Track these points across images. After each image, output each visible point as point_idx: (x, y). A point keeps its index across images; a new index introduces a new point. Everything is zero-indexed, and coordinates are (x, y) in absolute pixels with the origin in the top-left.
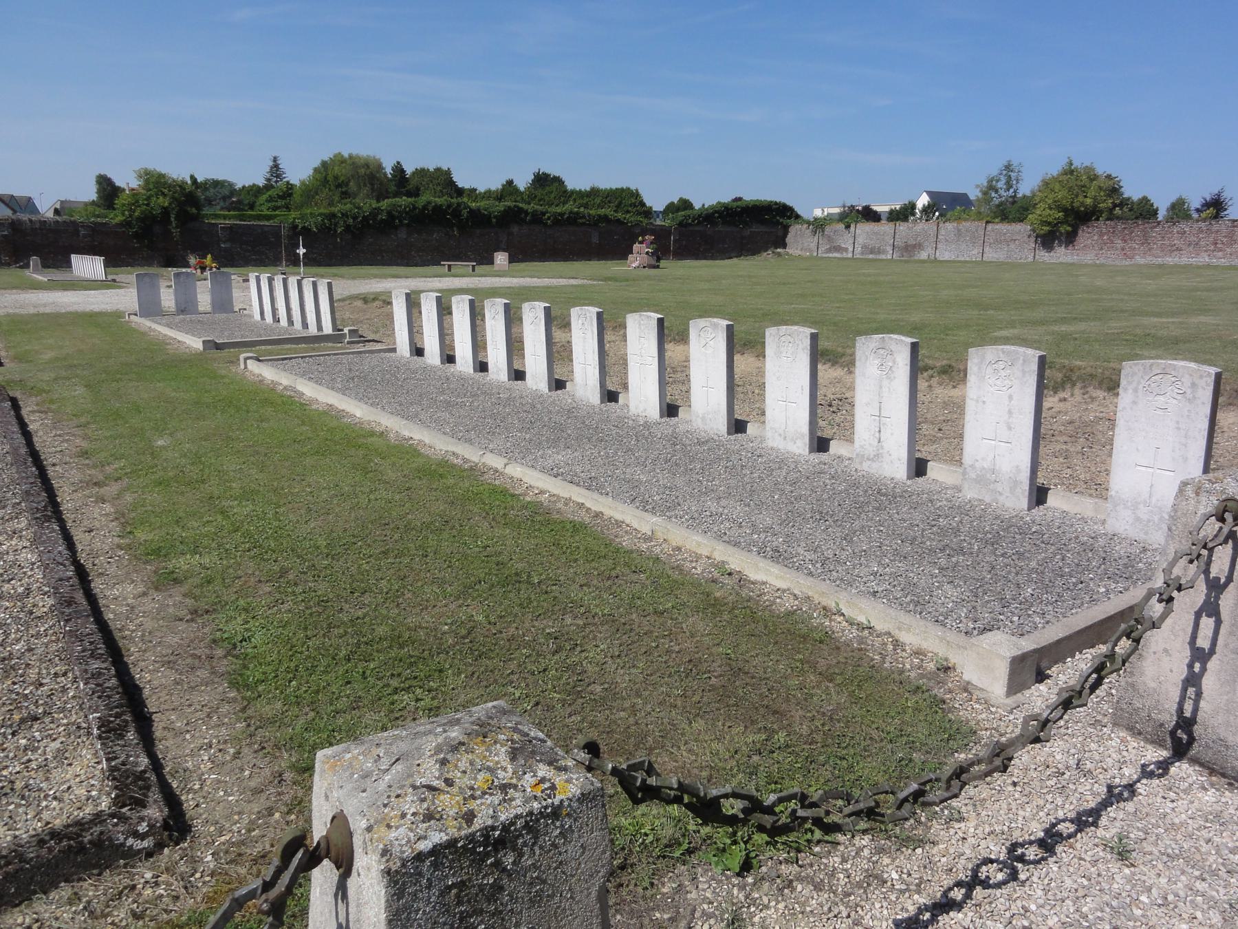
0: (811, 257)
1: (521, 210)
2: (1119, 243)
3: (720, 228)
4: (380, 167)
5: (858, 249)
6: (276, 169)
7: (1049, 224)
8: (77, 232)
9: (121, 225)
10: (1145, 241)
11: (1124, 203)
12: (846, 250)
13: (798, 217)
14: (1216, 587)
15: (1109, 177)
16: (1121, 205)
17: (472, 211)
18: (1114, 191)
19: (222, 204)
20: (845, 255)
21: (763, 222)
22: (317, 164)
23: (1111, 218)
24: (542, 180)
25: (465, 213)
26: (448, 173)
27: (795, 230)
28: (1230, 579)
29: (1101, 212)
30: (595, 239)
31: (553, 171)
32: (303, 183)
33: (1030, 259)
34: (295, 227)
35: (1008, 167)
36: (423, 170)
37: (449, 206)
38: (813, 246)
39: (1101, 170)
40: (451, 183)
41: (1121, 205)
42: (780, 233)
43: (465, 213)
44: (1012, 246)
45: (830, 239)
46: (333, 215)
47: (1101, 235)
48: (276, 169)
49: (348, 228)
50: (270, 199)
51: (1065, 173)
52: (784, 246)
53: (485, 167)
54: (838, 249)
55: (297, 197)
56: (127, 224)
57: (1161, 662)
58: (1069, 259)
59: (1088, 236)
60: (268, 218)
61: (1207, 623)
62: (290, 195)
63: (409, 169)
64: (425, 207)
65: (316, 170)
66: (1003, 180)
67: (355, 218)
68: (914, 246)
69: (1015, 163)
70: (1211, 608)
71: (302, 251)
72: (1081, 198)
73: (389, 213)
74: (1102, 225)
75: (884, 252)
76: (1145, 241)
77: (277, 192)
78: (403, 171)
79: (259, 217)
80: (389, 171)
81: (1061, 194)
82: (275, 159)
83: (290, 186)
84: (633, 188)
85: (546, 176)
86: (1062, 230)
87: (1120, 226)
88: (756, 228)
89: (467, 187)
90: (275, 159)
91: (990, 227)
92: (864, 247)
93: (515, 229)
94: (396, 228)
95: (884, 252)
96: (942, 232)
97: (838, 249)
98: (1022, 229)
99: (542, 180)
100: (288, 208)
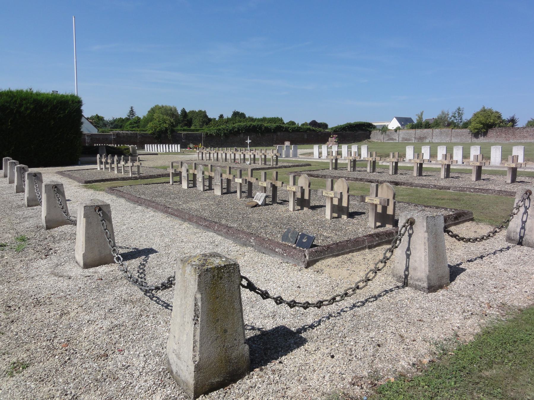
0: (381, 143)
1: (281, 127)
2: (504, 135)
3: (348, 132)
4: (176, 110)
5: (400, 139)
6: (132, 112)
7: (477, 129)
8: (137, 136)
9: (151, 134)
10: (514, 134)
11: (503, 121)
12: (396, 140)
13: (374, 127)
14: (526, 208)
15: (497, 112)
16: (502, 122)
17: (265, 127)
18: (499, 117)
19: (111, 126)
20: (395, 141)
21: (362, 130)
22: (149, 109)
23: (500, 127)
24: (236, 114)
25: (263, 128)
26: (205, 112)
27: (374, 133)
28: (529, 206)
29: (496, 124)
30: (306, 137)
31: (241, 111)
32: (144, 117)
33: (470, 142)
34: (207, 134)
35: (459, 109)
36: (193, 111)
37: (258, 125)
38: (382, 138)
39: (494, 110)
40: (206, 116)
41: (502, 122)
42: (368, 134)
43: (263, 128)
44: (463, 137)
45: (388, 136)
46: (220, 130)
47: (497, 133)
48: (132, 112)
49: (225, 134)
50: (131, 124)
51: (482, 111)
52: (369, 138)
53: (218, 109)
54: (392, 139)
55: (142, 123)
56: (153, 134)
57: (515, 224)
58: (485, 141)
59: (492, 133)
60: (197, 130)
61: (525, 216)
62: (139, 122)
63: (187, 111)
64: (250, 126)
65: (149, 112)
66: (457, 114)
67: (227, 130)
68: (423, 138)
69: (461, 108)
70: (526, 212)
71: (249, 141)
72: (489, 120)
73: (238, 129)
74: (497, 129)
75: (411, 140)
76: (514, 134)
77: (132, 121)
78: (185, 112)
79: (193, 130)
80: (179, 112)
81: (482, 119)
82: (132, 108)
83: (139, 119)
84: (280, 117)
85: (238, 113)
86: (482, 131)
87: (504, 129)
88: (360, 132)
89: (212, 118)
90: (132, 108)
91: (453, 130)
92: (403, 138)
93: (279, 134)
94: (240, 134)
95: (411, 140)
96: (434, 132)
97: (392, 139)
98: (467, 131)
99: (236, 114)
100: (138, 127)
